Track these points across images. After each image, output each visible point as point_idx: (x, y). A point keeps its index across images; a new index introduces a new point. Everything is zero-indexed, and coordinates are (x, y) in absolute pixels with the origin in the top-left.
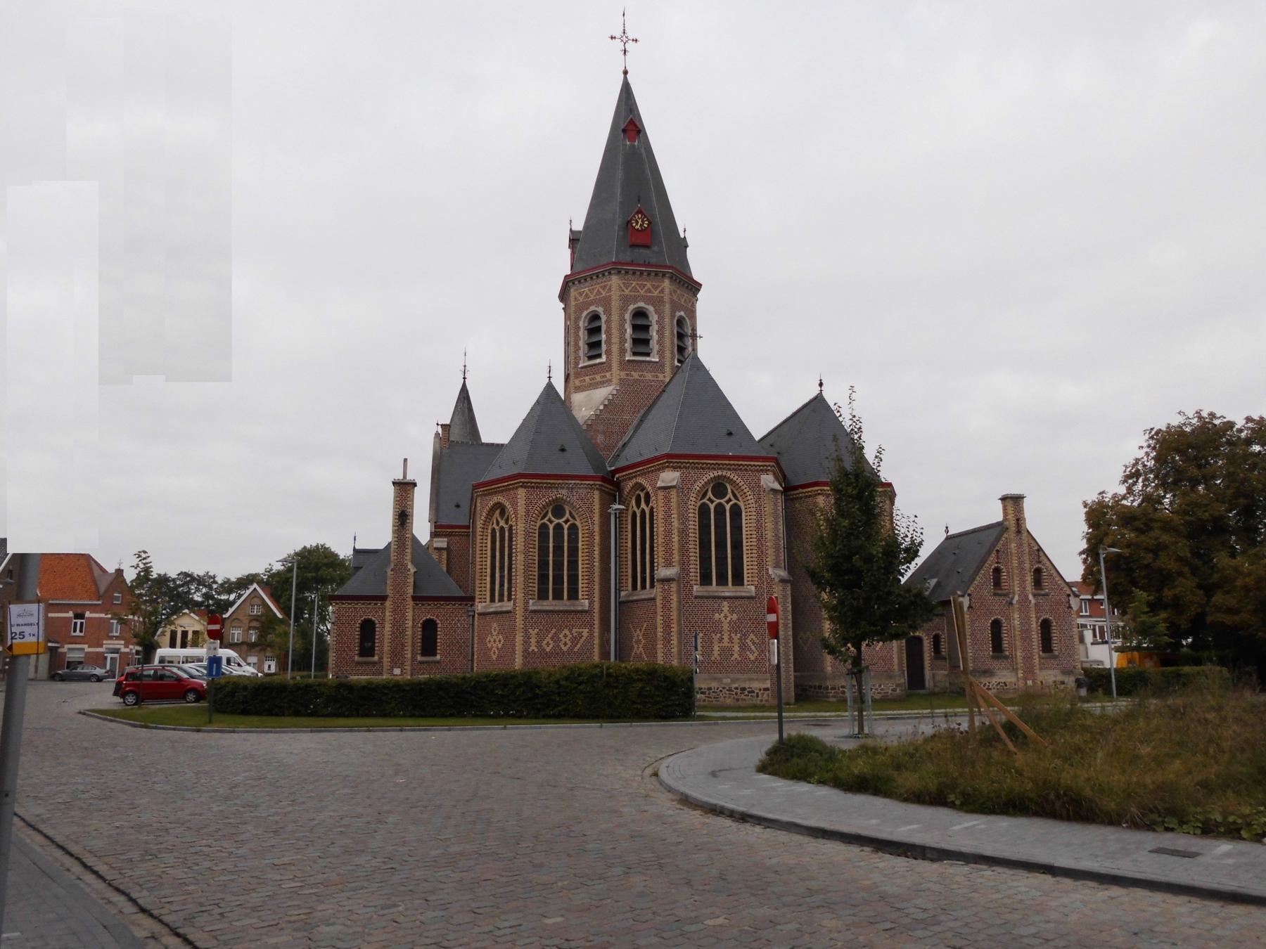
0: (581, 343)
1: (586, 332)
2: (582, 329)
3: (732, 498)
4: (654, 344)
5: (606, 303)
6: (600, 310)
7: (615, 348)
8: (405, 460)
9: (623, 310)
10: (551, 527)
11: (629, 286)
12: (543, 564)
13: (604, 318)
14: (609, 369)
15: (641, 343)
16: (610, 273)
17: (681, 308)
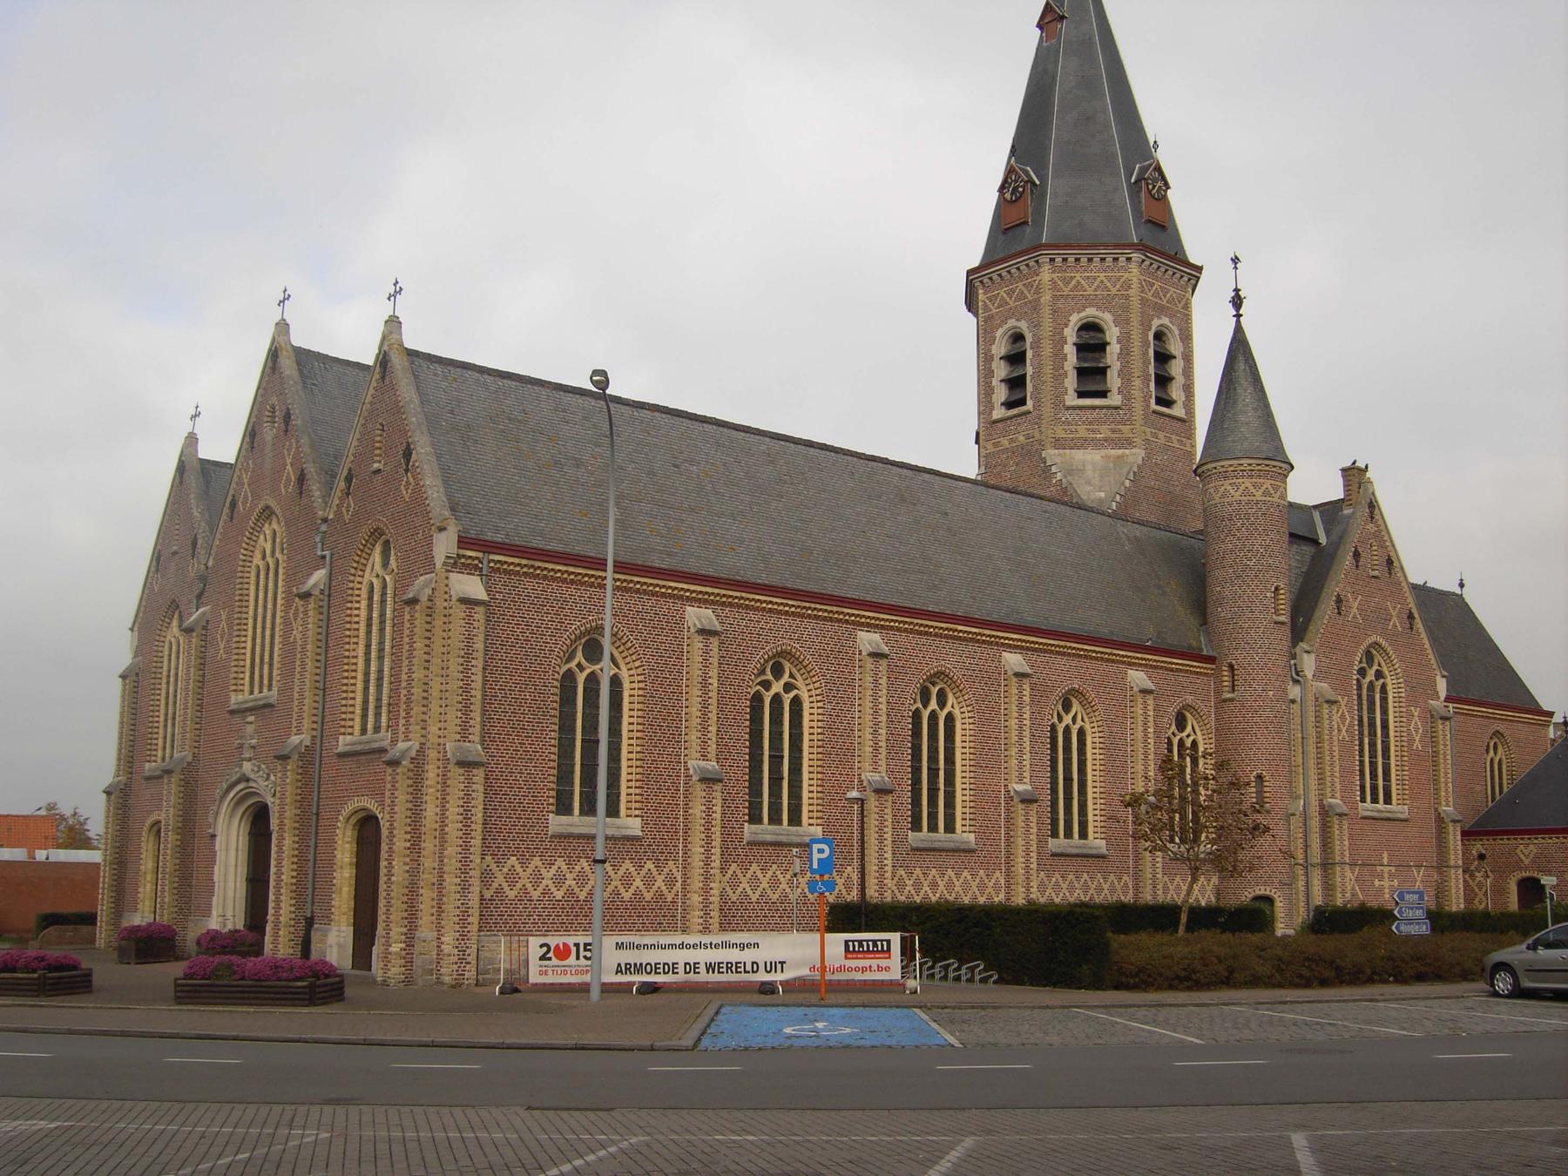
4: (1113, 380)
6: (1023, 326)
10: (581, 678)
11: (1075, 287)
13: (1029, 339)
15: (1092, 377)
17: (1161, 310)
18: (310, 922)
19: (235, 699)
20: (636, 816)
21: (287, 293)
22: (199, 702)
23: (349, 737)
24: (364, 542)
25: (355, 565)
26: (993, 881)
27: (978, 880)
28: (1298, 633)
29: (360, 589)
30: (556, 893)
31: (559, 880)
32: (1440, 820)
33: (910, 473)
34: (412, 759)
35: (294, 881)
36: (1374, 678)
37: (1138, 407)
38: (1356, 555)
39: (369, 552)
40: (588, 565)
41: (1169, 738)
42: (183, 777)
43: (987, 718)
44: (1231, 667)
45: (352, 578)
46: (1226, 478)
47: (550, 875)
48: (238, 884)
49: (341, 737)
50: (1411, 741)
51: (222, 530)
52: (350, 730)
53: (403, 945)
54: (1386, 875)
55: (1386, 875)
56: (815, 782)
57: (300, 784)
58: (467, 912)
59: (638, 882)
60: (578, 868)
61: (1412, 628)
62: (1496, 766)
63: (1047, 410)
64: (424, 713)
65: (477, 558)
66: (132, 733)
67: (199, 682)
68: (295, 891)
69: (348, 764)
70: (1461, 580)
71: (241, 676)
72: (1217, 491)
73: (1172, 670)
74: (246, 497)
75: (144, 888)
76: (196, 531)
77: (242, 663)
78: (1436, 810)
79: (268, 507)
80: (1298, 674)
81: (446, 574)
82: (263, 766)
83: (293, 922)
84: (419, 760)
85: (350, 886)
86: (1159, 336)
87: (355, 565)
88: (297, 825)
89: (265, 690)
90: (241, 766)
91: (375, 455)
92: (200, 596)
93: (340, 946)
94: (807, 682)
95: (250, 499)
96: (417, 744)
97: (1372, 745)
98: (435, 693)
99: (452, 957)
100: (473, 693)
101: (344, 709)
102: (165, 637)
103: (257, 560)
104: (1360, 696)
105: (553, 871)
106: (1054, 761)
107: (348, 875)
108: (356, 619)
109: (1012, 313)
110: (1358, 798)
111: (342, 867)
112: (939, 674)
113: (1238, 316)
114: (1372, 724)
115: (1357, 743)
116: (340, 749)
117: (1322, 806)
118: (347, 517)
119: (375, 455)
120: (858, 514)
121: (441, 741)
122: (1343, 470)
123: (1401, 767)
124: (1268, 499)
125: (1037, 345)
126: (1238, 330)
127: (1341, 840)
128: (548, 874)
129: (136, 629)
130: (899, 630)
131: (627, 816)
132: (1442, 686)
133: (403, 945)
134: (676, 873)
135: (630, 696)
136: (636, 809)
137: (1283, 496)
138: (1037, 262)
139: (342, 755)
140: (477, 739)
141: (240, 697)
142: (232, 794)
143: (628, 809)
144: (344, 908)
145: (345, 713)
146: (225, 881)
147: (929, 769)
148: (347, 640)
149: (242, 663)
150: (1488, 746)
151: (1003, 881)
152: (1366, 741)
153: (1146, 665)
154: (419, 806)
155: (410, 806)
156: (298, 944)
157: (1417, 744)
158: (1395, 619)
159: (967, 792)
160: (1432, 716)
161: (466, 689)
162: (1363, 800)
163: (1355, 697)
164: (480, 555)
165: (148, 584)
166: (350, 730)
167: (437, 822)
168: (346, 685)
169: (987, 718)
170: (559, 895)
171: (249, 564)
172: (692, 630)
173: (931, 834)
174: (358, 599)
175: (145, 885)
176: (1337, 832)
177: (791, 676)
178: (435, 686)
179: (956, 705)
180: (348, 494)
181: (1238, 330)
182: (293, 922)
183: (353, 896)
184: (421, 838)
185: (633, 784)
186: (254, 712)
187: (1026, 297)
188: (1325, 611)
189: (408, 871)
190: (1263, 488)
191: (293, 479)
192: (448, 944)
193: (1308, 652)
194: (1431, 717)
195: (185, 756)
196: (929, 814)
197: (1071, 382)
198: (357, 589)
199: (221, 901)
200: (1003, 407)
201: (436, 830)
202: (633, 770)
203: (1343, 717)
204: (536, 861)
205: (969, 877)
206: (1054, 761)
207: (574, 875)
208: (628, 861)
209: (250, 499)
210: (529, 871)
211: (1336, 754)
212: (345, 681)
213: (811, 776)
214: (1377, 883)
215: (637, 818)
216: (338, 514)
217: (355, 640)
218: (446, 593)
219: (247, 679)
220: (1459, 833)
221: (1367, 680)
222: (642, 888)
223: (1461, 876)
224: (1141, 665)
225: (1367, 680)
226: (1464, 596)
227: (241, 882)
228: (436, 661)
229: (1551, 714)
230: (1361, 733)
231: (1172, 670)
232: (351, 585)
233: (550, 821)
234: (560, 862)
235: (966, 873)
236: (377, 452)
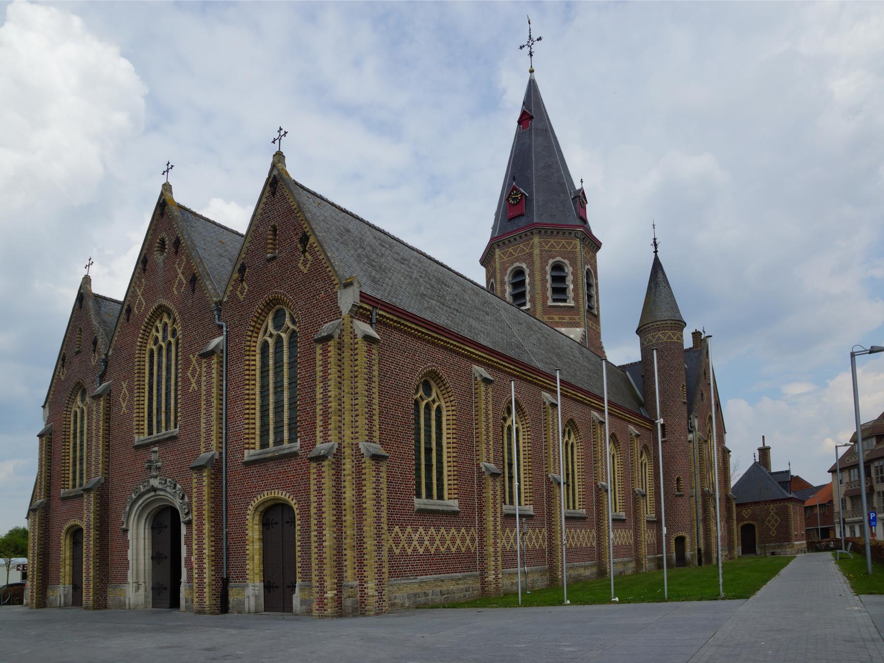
1: (511, 286)
2: (507, 284)
4: (570, 294)
5: (529, 258)
7: (539, 298)
8: (763, 437)
9: (544, 262)
13: (527, 272)
15: (560, 291)
16: (532, 233)
19: (138, 439)
20: (455, 499)
21: (91, 261)
22: (107, 444)
23: (252, 452)
24: (260, 311)
29: (255, 346)
34: (334, 454)
39: (263, 319)
42: (99, 493)
46: (659, 330)
48: (147, 561)
49: (246, 451)
51: (119, 330)
52: (252, 446)
53: (335, 592)
56: (527, 479)
57: (213, 486)
58: (382, 564)
63: (539, 308)
64: (340, 421)
65: (369, 310)
66: (49, 471)
67: (106, 430)
68: (215, 561)
69: (254, 470)
71: (142, 423)
74: (140, 303)
75: (65, 569)
76: (95, 335)
77: (141, 415)
80: (691, 427)
82: (168, 480)
83: (214, 582)
84: (338, 456)
85: (260, 554)
87: (252, 328)
88: (213, 515)
89: (164, 431)
90: (148, 482)
91: (268, 249)
93: (256, 597)
94: (522, 419)
95: (144, 304)
96: (337, 444)
98: (347, 406)
99: (374, 598)
102: (71, 408)
103: (151, 345)
107: (258, 547)
108: (253, 368)
111: (253, 542)
113: (656, 252)
116: (246, 459)
119: (268, 249)
121: (354, 442)
122: (693, 333)
125: (532, 275)
126: (656, 260)
128: (415, 537)
129: (47, 406)
131: (449, 499)
134: (475, 535)
135: (447, 420)
136: (454, 494)
139: (248, 464)
140: (377, 441)
141: (142, 437)
142: (140, 502)
143: (449, 494)
144: (257, 570)
148: (247, 382)
154: (340, 490)
156: (218, 597)
159: (581, 487)
161: (370, 403)
164: (371, 308)
165: (56, 377)
166: (252, 446)
167: (354, 501)
171: (144, 348)
174: (254, 353)
175: (65, 567)
178: (347, 401)
180: (242, 281)
181: (656, 260)
183: (262, 561)
184: (342, 513)
185: (452, 478)
186: (157, 445)
187: (525, 251)
191: (184, 281)
192: (372, 589)
193: (696, 417)
195: (100, 479)
198: (253, 346)
201: (353, 507)
202: (452, 469)
208: (453, 528)
209: (144, 304)
213: (526, 476)
215: (455, 500)
217: (253, 382)
218: (351, 333)
219: (146, 425)
227: (148, 559)
228: (347, 383)
233: (415, 501)
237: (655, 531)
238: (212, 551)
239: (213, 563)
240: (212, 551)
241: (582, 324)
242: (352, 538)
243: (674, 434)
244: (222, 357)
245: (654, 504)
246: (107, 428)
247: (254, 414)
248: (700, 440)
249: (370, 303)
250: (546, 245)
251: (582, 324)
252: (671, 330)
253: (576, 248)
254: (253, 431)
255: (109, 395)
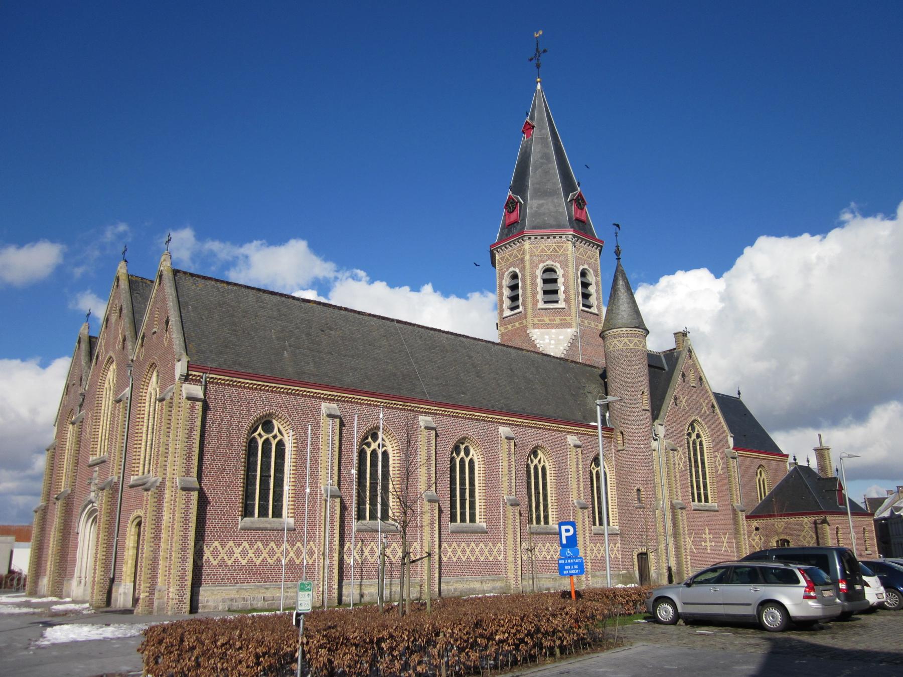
0: (505, 298)
3: (278, 434)
4: (561, 295)
9: (534, 266)
12: (504, 423)
13: (520, 276)
14: (525, 317)
15: (551, 293)
18: (112, 580)
20: (291, 517)
23: (136, 477)
25: (143, 383)
26: (497, 548)
27: (488, 548)
28: (655, 417)
29: (145, 396)
30: (242, 561)
31: (244, 554)
32: (734, 511)
33: (453, 337)
34: (157, 487)
35: (104, 557)
36: (695, 438)
37: (573, 310)
38: (683, 375)
40: (264, 380)
41: (591, 471)
43: (491, 462)
44: (622, 433)
45: (141, 390)
46: (615, 338)
47: (239, 551)
49: (132, 477)
50: (717, 470)
52: (137, 473)
53: (147, 594)
54: (708, 540)
55: (708, 540)
57: (110, 503)
59: (292, 554)
60: (256, 547)
61: (714, 412)
62: (762, 482)
63: (530, 311)
65: (199, 376)
70: (739, 391)
71: (96, 446)
72: (611, 345)
73: (590, 435)
74: (103, 353)
78: (732, 505)
79: (111, 357)
80: (656, 435)
81: (181, 385)
83: (102, 581)
84: (161, 488)
85: (132, 560)
86: (584, 274)
87: (143, 383)
88: (107, 526)
92: (81, 406)
97: (697, 472)
100: (193, 449)
101: (134, 461)
104: (689, 447)
105: (241, 548)
106: (529, 484)
108: (143, 412)
109: (512, 265)
110: (691, 500)
111: (128, 549)
112: (464, 438)
114: (696, 461)
115: (689, 471)
117: (672, 504)
118: (141, 358)
120: (423, 356)
123: (712, 483)
124: (636, 347)
125: (523, 280)
127: (683, 522)
128: (238, 551)
129: (56, 425)
130: (442, 415)
132: (731, 441)
133: (147, 594)
134: (314, 548)
137: (645, 346)
138: (523, 240)
139: (132, 487)
141: (95, 458)
144: (128, 573)
145: (134, 463)
146: (82, 559)
147: (460, 489)
149: (96, 440)
150: (757, 473)
151: (502, 548)
152: (693, 470)
153: (577, 433)
155: (155, 513)
157: (720, 471)
158: (705, 408)
160: (727, 457)
162: (693, 500)
163: (686, 447)
164: (201, 374)
168: (136, 448)
169: (491, 462)
170: (244, 562)
172: (324, 415)
173: (462, 524)
174: (144, 401)
176: (681, 518)
177: (383, 440)
179: (475, 455)
180: (142, 346)
182: (102, 581)
188: (669, 403)
189: (152, 551)
190: (634, 342)
194: (725, 457)
196: (461, 513)
197: (540, 296)
199: (79, 569)
200: (509, 310)
201: (169, 527)
203: (680, 458)
204: (231, 543)
205: (483, 547)
206: (529, 484)
207: (253, 551)
210: (226, 549)
211: (678, 477)
212: (135, 446)
214: (703, 544)
216: (138, 357)
220: (744, 517)
221: (692, 438)
222: (294, 557)
223: (747, 539)
224: (574, 433)
225: (692, 438)
226: (741, 399)
229: (787, 456)
230: (690, 466)
231: (590, 435)
232: (141, 394)
234: (245, 544)
235: (481, 544)
236: (156, 323)
237: (618, 545)
238: (103, 555)
239: (103, 565)
240: (103, 555)
241: (574, 324)
242: (165, 552)
243: (631, 442)
244: (127, 403)
245: (617, 515)
246: (78, 449)
247: (140, 448)
248: (666, 449)
249: (201, 370)
250: (537, 250)
251: (574, 324)
252: (628, 336)
253: (568, 250)
254: (138, 461)
255: (81, 422)
